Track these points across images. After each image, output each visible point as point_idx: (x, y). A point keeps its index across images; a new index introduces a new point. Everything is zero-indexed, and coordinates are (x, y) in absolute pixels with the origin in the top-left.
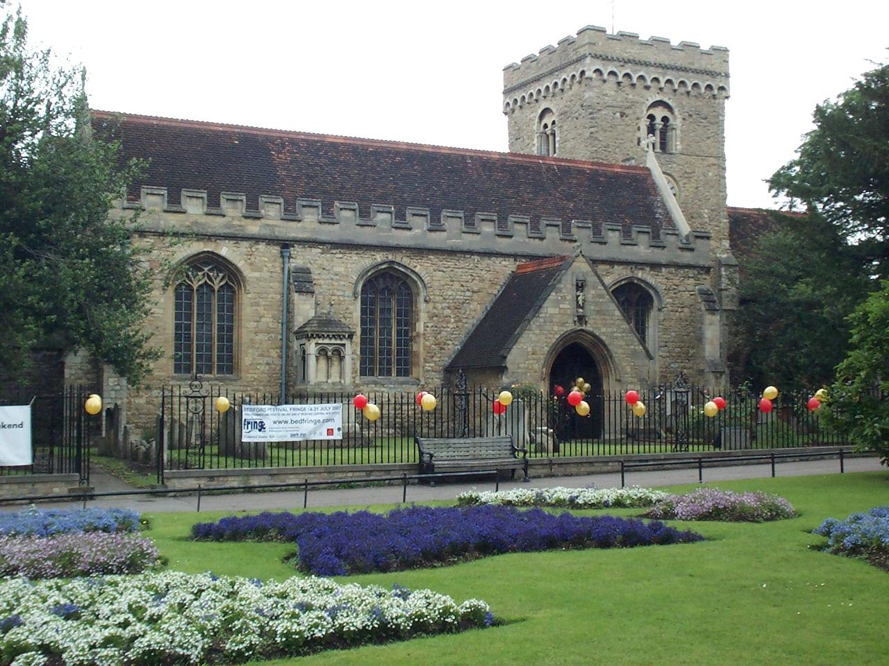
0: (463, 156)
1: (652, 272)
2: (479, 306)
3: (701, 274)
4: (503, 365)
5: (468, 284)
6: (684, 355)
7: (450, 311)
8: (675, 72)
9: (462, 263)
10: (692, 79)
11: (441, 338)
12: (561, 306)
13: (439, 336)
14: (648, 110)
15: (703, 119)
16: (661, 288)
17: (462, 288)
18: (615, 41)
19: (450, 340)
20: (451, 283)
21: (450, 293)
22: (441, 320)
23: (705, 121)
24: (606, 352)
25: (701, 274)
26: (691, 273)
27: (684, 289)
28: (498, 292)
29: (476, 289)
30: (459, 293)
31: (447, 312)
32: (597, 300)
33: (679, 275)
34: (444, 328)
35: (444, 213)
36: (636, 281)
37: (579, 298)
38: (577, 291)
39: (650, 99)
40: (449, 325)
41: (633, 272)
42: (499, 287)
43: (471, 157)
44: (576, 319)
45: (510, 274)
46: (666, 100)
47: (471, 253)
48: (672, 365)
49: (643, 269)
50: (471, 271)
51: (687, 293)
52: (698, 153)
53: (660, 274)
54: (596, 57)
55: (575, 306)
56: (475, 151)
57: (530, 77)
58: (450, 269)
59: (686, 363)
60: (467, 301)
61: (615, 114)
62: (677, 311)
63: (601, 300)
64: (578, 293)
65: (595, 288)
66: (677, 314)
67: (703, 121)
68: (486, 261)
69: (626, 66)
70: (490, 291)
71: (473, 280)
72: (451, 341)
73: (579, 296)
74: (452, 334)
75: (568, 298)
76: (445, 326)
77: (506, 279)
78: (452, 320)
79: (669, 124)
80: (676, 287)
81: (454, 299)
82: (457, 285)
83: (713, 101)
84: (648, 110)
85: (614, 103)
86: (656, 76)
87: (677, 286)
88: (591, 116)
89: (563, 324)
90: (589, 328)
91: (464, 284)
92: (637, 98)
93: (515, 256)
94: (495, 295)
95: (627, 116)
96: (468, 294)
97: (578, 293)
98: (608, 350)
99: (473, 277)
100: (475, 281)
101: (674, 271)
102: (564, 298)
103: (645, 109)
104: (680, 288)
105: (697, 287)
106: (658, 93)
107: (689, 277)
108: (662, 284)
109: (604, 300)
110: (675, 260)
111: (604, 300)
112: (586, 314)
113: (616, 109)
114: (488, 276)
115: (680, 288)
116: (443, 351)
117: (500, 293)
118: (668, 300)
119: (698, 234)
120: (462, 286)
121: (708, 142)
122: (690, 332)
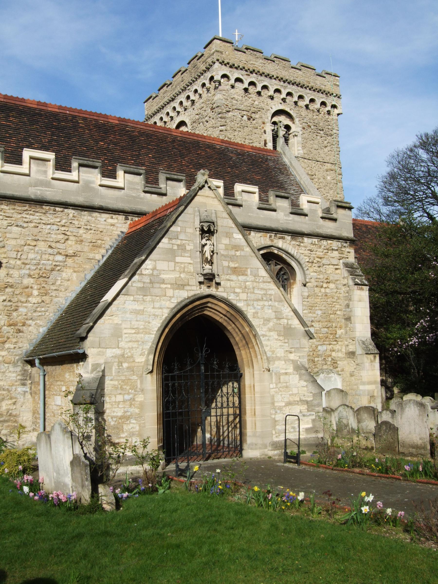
0: (74, 117)
1: (293, 242)
2: (75, 275)
3: (345, 247)
4: (81, 351)
5: (58, 245)
6: (331, 337)
7: (32, 280)
8: (295, 87)
9: (50, 218)
10: (309, 95)
11: (18, 316)
12: (178, 259)
13: (15, 314)
14: (272, 117)
15: (320, 130)
16: (304, 260)
17: (50, 251)
18: (241, 53)
19: (31, 319)
20: (34, 243)
21: (31, 256)
22: (17, 292)
23: (321, 132)
24: (247, 329)
25: (345, 247)
26: (335, 244)
27: (329, 263)
28: (103, 256)
29: (70, 252)
30: (47, 256)
31: (27, 281)
32: (232, 253)
33: (323, 247)
34: (23, 302)
35: (25, 149)
36: (276, 252)
37: (207, 248)
38: (202, 239)
39: (273, 107)
40: (30, 299)
41: (272, 241)
42: (103, 251)
43: (85, 119)
44: (202, 279)
45: (119, 236)
46: (288, 109)
47: (65, 205)
48: (319, 348)
49: (283, 238)
50: (63, 229)
51: (332, 266)
52: (318, 159)
53: (302, 244)
54: (222, 63)
55: (199, 260)
56: (91, 113)
57: (166, 99)
58: (33, 225)
59: (335, 345)
60: (59, 268)
61: (243, 117)
62: (322, 287)
63: (238, 253)
64: (204, 241)
65: (229, 235)
66: (323, 290)
67: (319, 131)
68: (86, 216)
69: (251, 75)
70: (91, 256)
71: (67, 239)
72: (33, 320)
73: (206, 244)
74: (35, 311)
75: (188, 248)
76: (24, 299)
77: (114, 240)
78: (35, 293)
79: (291, 132)
80: (319, 260)
81: (39, 264)
82: (42, 246)
83: (327, 116)
84: (272, 117)
85: (242, 107)
86: (279, 87)
87: (321, 258)
88: (220, 115)
89: (182, 286)
90: (220, 292)
91: (53, 245)
92: (262, 105)
93: (126, 213)
94: (99, 261)
95: (254, 120)
96: (60, 258)
97: (204, 241)
98: (250, 325)
99: (66, 237)
100: (69, 242)
101: (317, 243)
102: (182, 248)
103: (270, 116)
104: (324, 261)
105: (341, 261)
106: (281, 103)
107: (333, 249)
108: (305, 256)
109: (243, 253)
110: (317, 230)
111: (243, 253)
112: (215, 272)
113: (245, 113)
114: (88, 236)
115: (324, 261)
116: (20, 334)
117: (105, 259)
118: (312, 274)
119: (340, 204)
120: (50, 247)
121: (326, 150)
122: (337, 311)
